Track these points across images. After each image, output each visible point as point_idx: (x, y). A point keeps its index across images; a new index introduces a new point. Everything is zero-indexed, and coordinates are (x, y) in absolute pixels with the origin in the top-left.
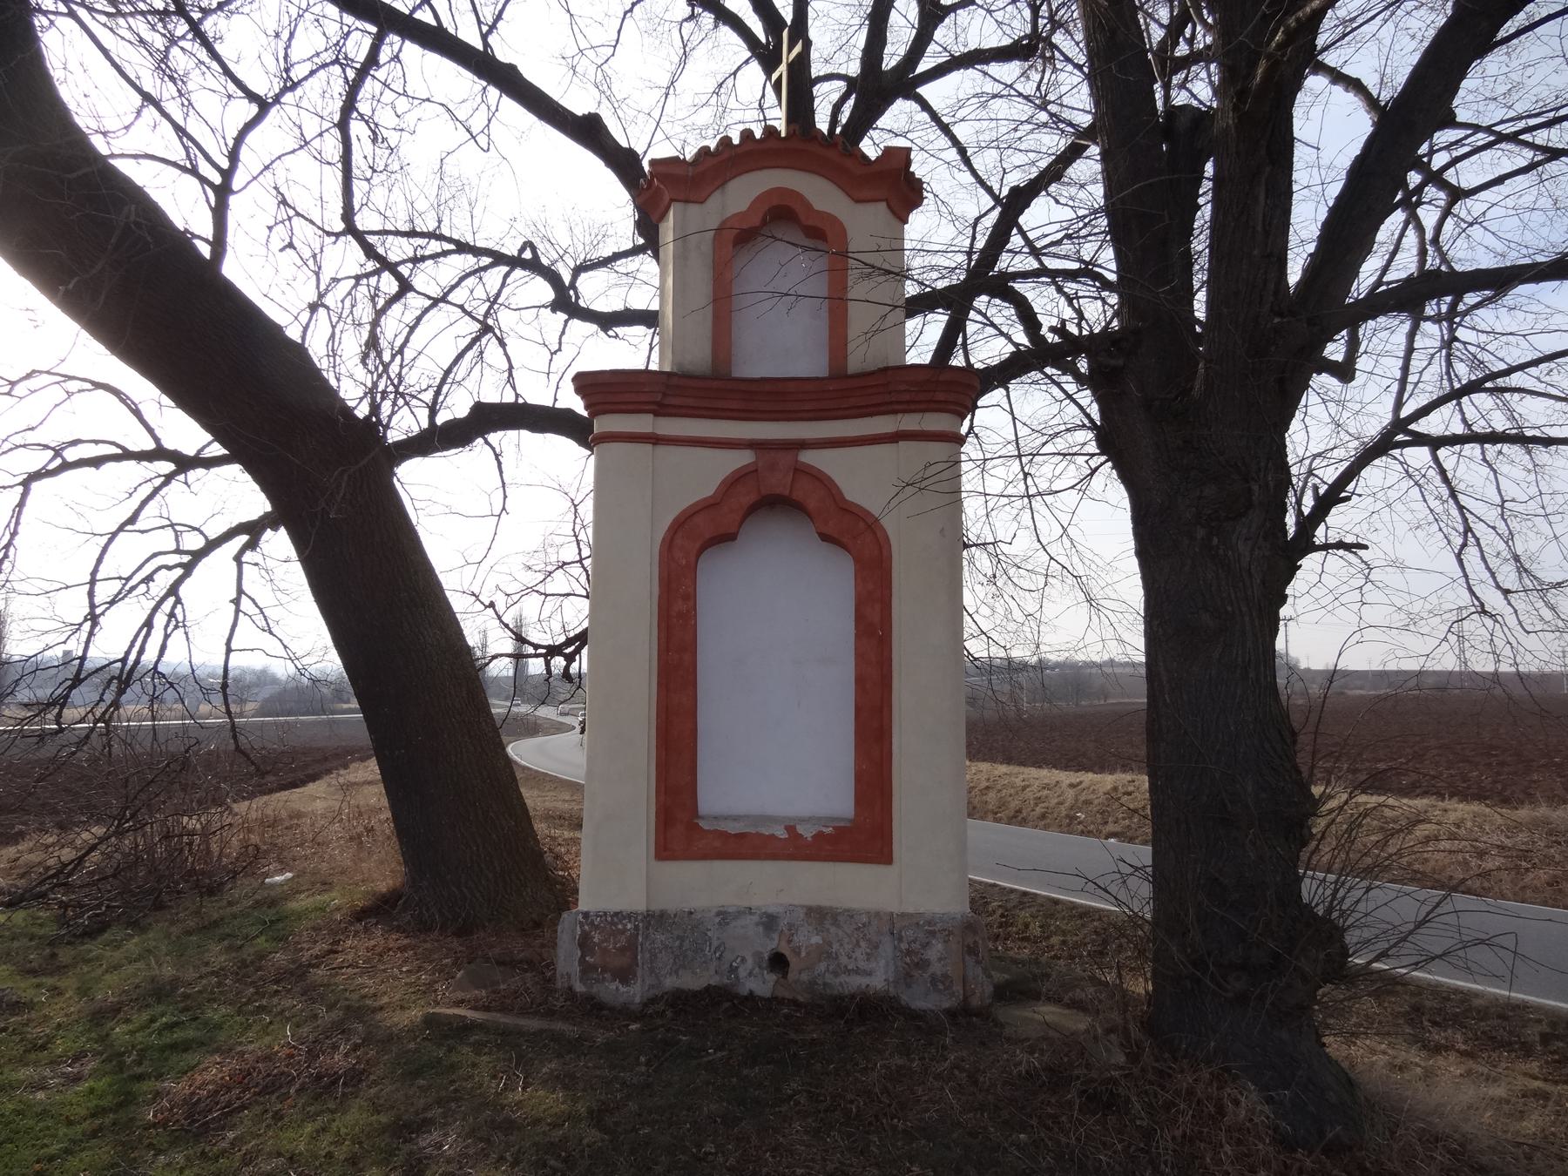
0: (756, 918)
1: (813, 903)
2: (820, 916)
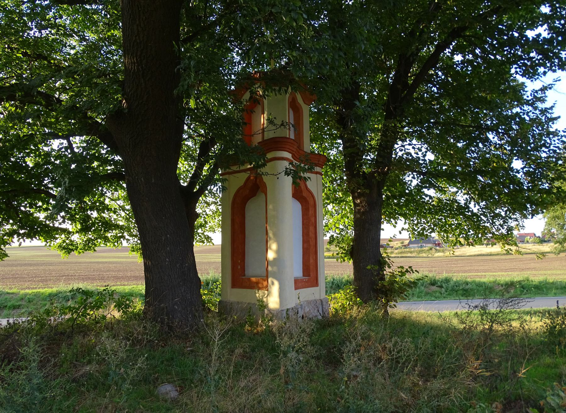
2: (309, 302)
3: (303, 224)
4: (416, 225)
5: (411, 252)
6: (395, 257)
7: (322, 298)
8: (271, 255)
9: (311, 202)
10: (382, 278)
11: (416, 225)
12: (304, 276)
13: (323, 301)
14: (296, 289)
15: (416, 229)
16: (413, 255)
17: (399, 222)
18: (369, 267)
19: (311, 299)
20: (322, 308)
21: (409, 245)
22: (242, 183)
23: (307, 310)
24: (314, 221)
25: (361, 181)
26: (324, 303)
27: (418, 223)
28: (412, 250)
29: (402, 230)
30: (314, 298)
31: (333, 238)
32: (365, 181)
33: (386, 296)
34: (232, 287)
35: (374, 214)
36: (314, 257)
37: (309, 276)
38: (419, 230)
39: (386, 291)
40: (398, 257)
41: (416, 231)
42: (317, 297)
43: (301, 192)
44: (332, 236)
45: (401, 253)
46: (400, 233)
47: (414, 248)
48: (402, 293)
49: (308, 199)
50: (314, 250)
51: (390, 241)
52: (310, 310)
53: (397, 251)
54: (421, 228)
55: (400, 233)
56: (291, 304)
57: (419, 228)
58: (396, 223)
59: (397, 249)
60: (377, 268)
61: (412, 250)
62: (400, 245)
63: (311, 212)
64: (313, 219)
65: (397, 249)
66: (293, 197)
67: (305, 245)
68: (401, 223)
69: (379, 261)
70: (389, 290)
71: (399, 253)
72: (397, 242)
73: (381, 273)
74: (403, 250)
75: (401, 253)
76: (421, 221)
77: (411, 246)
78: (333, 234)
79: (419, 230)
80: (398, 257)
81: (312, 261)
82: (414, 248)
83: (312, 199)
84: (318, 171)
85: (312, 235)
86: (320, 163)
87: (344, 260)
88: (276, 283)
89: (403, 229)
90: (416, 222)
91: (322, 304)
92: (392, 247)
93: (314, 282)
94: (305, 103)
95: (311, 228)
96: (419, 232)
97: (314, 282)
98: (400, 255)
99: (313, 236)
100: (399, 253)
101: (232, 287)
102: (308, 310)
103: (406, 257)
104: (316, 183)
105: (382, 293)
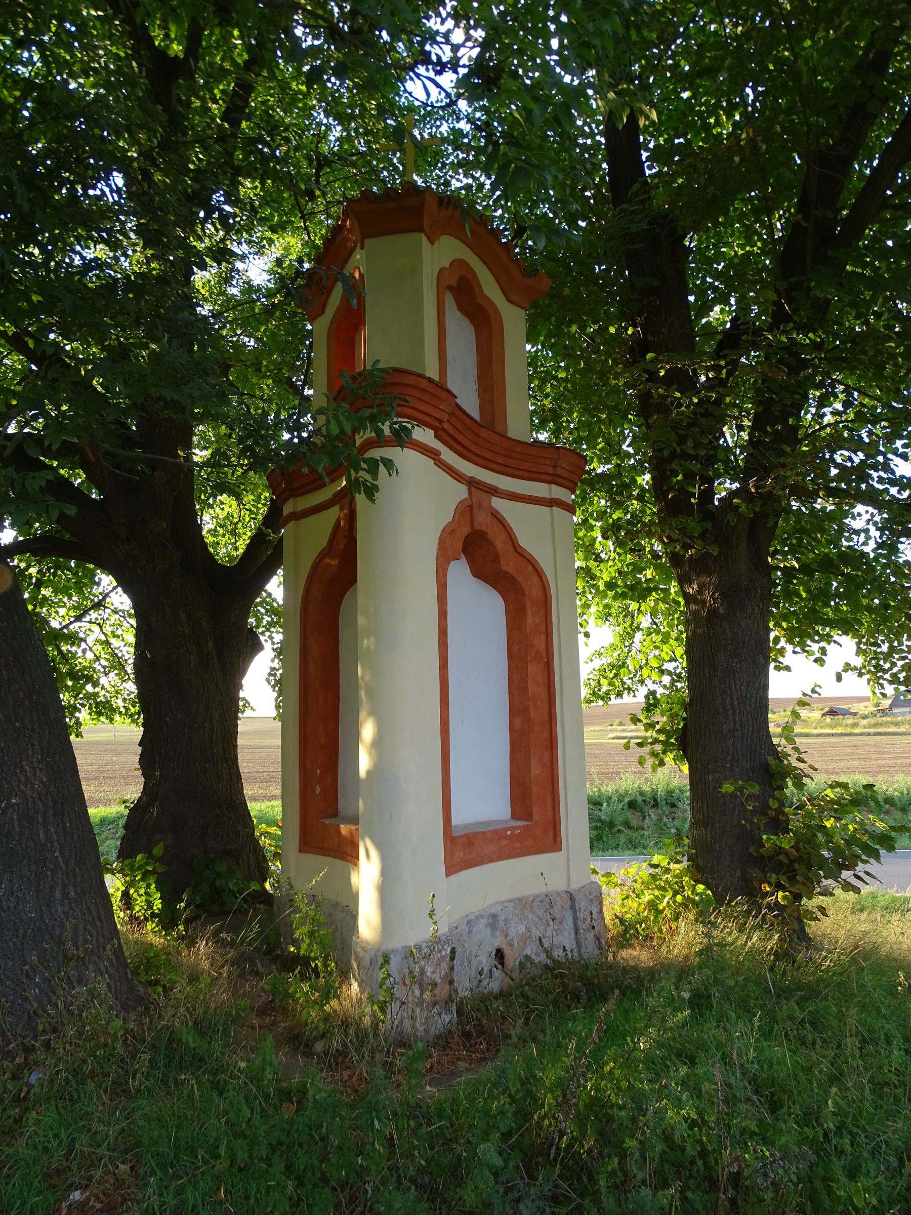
0: (485, 921)
1: (518, 895)
2: (523, 904)
3: (511, 657)
4: (888, 656)
5: (897, 724)
6: (861, 734)
7: (574, 886)
8: (365, 762)
9: (534, 591)
10: (779, 825)
11: (888, 656)
12: (514, 816)
13: (577, 898)
14: (450, 870)
15: (887, 666)
16: (902, 729)
17: (831, 648)
18: (728, 788)
19: (535, 892)
20: (575, 919)
21: (890, 708)
22: (322, 542)
23: (517, 929)
24: (542, 648)
25: (693, 525)
26: (582, 904)
27: (892, 650)
28: (899, 719)
29: (845, 671)
30: (544, 890)
31: (655, 698)
32: (708, 525)
33: (792, 879)
34: (301, 851)
35: (743, 624)
36: (546, 760)
37: (528, 817)
38: (895, 670)
39: (792, 862)
40: (869, 734)
41: (885, 671)
42: (557, 883)
43: (496, 558)
44: (653, 693)
45: (875, 725)
46: (839, 678)
47: (903, 714)
48: (846, 868)
49: (520, 579)
50: (545, 735)
51: (802, 704)
52: (528, 929)
53: (865, 722)
54: (900, 663)
55: (839, 678)
56: (417, 932)
57: (894, 665)
58: (823, 651)
59: (865, 717)
60: (755, 789)
61: (899, 719)
62: (872, 709)
63: (531, 620)
64: (539, 642)
65: (865, 717)
66: (475, 576)
67: (518, 722)
68: (844, 649)
69: (766, 766)
70: (800, 859)
71: (870, 726)
72: (865, 704)
73: (773, 804)
74: (880, 720)
75: (875, 725)
76: (900, 644)
77: (895, 710)
78: (652, 687)
79: (895, 670)
80: (869, 734)
81: (536, 770)
82: (903, 714)
83: (535, 579)
84: (554, 496)
85: (535, 689)
86: (559, 471)
87: (662, 763)
88: (374, 853)
89: (848, 667)
90: (885, 648)
91: (573, 907)
92: (855, 714)
93: (549, 838)
94: (509, 300)
95: (534, 669)
96: (895, 676)
97: (549, 838)
98: (872, 730)
99: (543, 693)
100: (870, 726)
101: (301, 851)
102: (522, 928)
103: (886, 734)
104: (531, 525)
105: (779, 868)
